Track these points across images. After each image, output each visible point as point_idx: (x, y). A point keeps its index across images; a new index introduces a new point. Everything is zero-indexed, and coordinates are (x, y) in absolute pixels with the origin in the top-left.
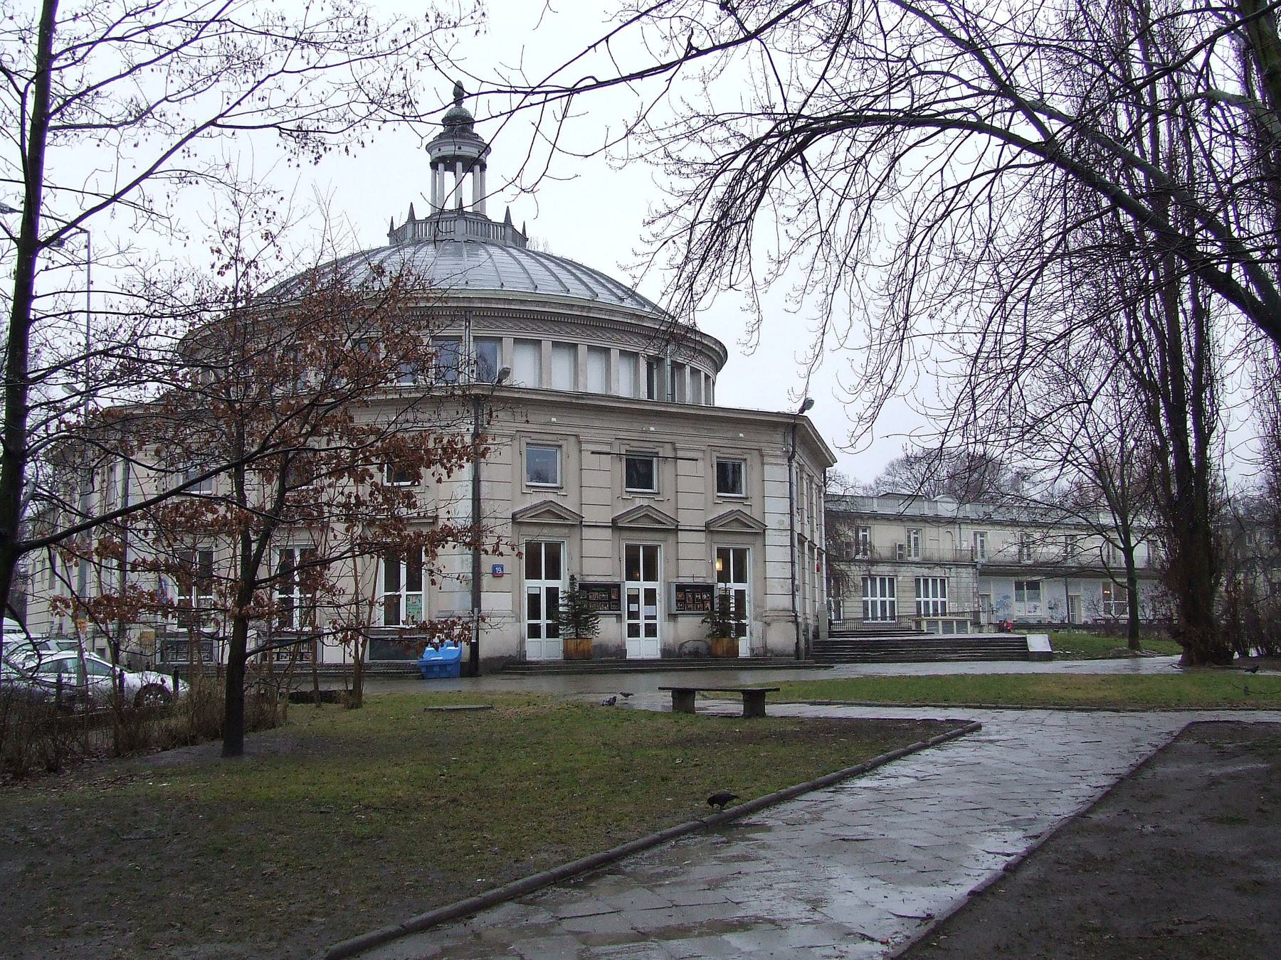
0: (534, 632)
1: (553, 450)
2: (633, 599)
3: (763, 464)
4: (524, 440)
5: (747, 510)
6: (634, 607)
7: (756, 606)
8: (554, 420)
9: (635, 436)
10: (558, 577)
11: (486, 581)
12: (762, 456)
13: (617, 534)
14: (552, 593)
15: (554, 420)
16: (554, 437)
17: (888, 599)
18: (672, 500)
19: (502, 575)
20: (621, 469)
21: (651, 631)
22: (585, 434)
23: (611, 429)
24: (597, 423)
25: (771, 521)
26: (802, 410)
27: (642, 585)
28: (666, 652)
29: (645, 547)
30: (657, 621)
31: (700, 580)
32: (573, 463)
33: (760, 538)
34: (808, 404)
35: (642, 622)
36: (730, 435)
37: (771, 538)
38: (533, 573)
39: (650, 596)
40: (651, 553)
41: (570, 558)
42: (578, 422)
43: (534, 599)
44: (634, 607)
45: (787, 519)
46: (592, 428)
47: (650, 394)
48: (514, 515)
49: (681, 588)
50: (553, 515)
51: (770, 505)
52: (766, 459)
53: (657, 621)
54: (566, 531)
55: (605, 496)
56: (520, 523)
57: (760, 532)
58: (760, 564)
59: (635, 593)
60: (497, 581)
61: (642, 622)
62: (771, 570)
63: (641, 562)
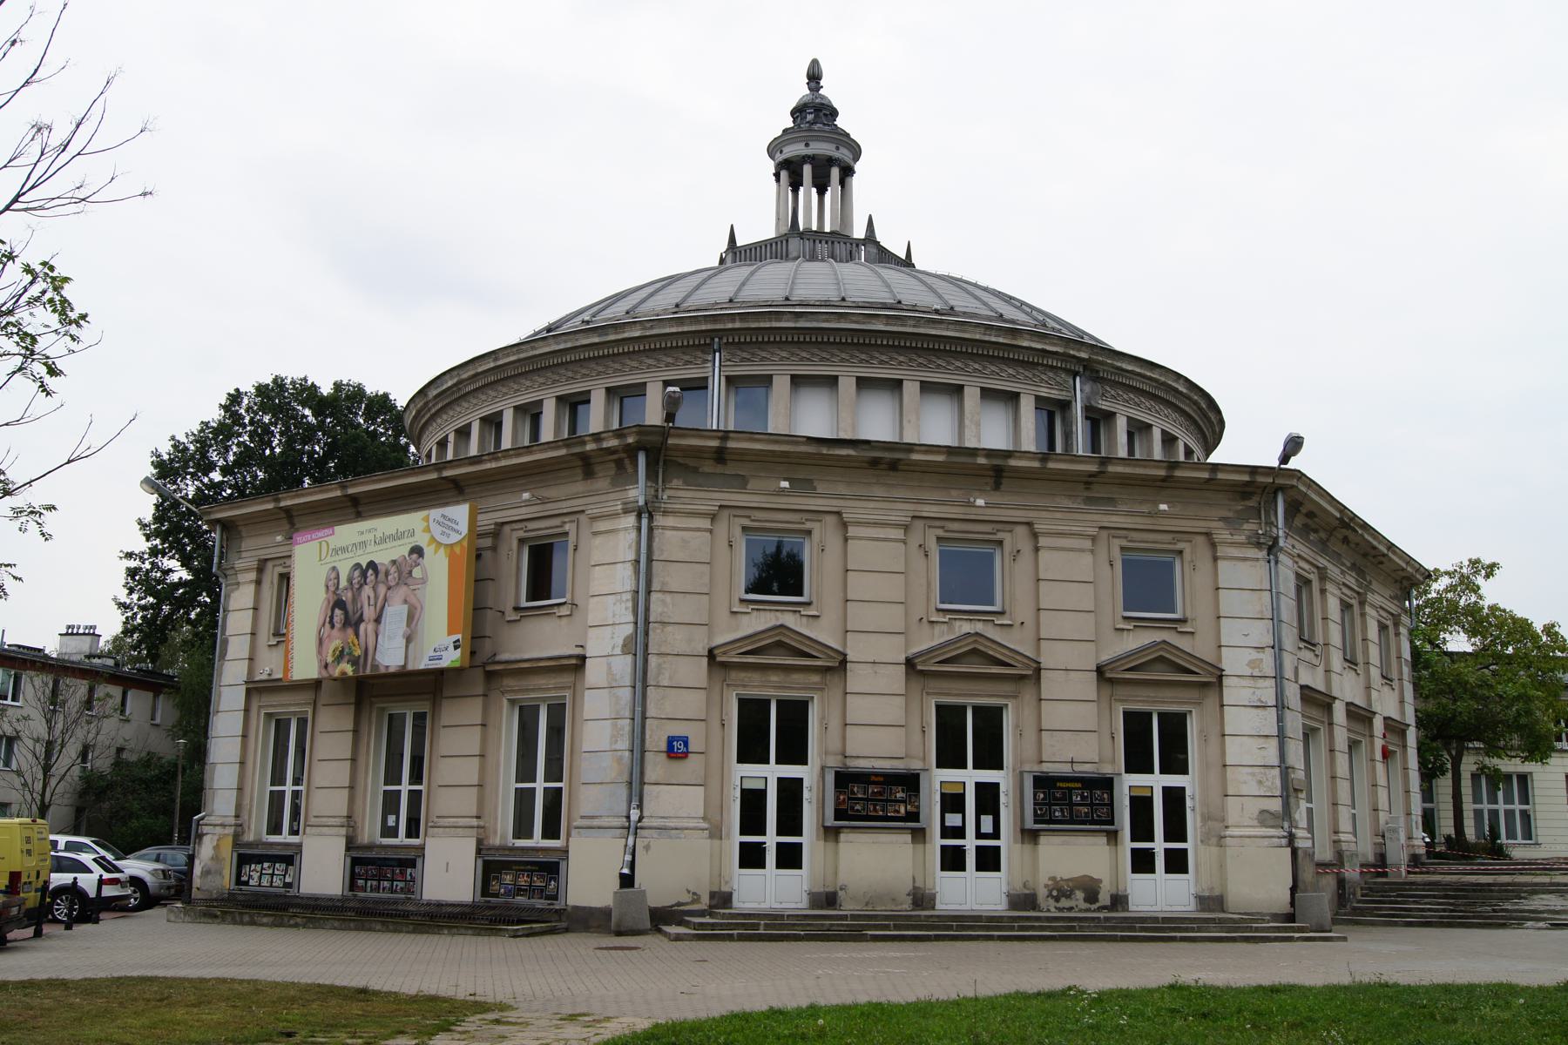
0: (752, 857)
1: (986, 549)
2: (953, 802)
3: (1215, 559)
4: (932, 534)
5: (1183, 643)
6: (953, 820)
7: (1206, 818)
8: (1163, 507)
9: (1139, 522)
10: (802, 759)
11: (657, 766)
12: (1213, 545)
13: (1107, 690)
14: (791, 791)
15: (1163, 507)
16: (988, 528)
17: (1517, 807)
18: (1030, 623)
19: (685, 755)
20: (1113, 582)
21: (989, 860)
22: (853, 510)
23: (905, 500)
24: (879, 491)
25: (1232, 662)
26: (1285, 458)
27: (970, 777)
28: (1023, 901)
29: (1161, 715)
30: (1001, 842)
31: (1087, 768)
32: (832, 562)
33: (834, 680)
34: (1293, 445)
35: (970, 843)
36: (1145, 508)
37: (1234, 692)
38: (751, 751)
39: (988, 797)
40: (990, 721)
41: (1020, 734)
42: (842, 489)
43: (752, 802)
44: (953, 820)
45: (1268, 658)
46: (868, 498)
47: (1131, 450)
48: (711, 651)
49: (1043, 782)
50: (976, 658)
51: (1231, 632)
52: (1042, 541)
53: (1001, 842)
54: (815, 678)
55: (892, 617)
56: (1111, 681)
57: (1212, 681)
58: (1214, 739)
59: (759, 785)
60: (677, 766)
61: (970, 843)
62: (1235, 751)
63: (969, 735)
